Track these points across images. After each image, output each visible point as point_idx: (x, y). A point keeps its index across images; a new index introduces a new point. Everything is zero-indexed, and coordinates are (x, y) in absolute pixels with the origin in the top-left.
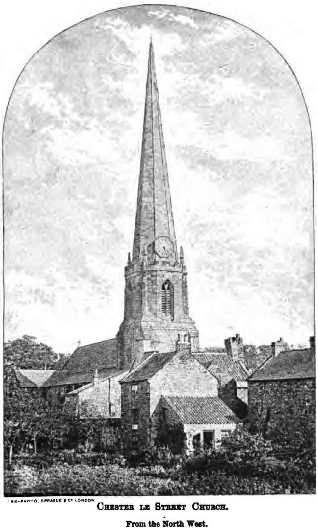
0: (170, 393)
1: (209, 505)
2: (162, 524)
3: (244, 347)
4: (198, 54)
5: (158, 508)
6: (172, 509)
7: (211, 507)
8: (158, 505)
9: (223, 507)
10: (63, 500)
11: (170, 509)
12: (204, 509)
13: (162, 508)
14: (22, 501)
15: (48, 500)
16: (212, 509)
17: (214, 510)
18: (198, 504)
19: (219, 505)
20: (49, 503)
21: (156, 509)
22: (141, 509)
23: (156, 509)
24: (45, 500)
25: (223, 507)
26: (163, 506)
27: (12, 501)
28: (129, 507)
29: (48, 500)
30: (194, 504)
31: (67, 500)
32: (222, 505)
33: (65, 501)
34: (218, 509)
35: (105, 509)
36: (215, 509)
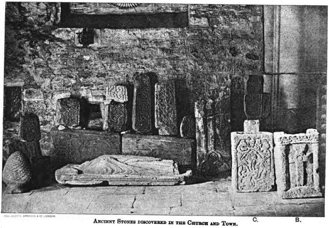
0: (135, 32)
1: (198, 222)
2: (116, 221)
3: (285, 49)
4: (122, 5)
5: (119, 222)
6: (161, 223)
7: (199, 223)
8: (119, 220)
9: (54, 216)
10: (36, 216)
11: (160, 223)
12: (194, 224)
13: (121, 222)
14: (119, 221)
15: (28, 216)
16: (199, 224)
17: (200, 225)
18: (191, 221)
19: (204, 223)
20: (28, 218)
21: (296, 221)
22: (169, 224)
23: (118, 223)
24: (26, 216)
25: (54, 216)
26: (122, 221)
27: (6, 216)
28: (157, 222)
29: (28, 216)
30: (189, 221)
31: (39, 216)
32: (206, 223)
33: (38, 216)
34: (203, 225)
35: (192, 224)
36: (201, 224)
